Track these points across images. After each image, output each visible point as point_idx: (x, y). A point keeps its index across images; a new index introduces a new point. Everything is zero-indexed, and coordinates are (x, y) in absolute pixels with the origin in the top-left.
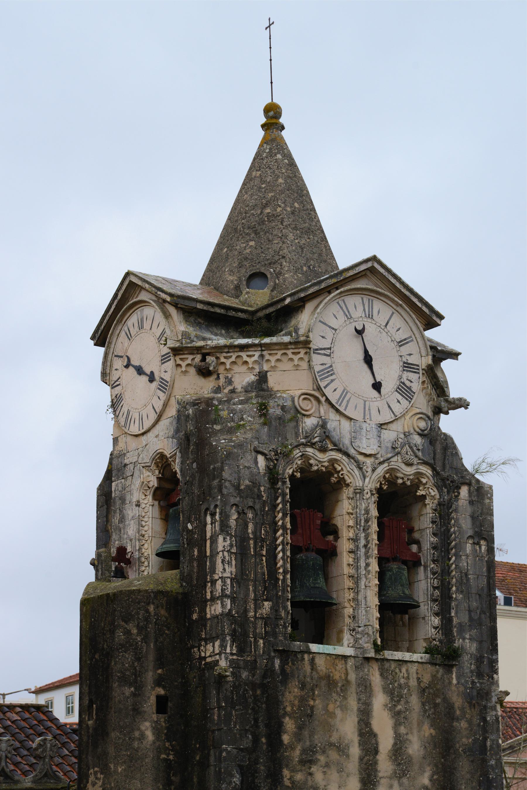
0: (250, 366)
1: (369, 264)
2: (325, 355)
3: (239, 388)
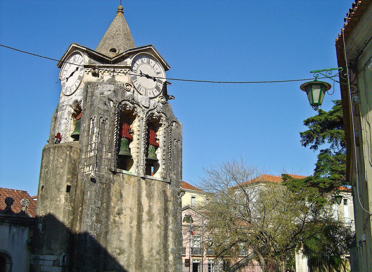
1: (150, 47)
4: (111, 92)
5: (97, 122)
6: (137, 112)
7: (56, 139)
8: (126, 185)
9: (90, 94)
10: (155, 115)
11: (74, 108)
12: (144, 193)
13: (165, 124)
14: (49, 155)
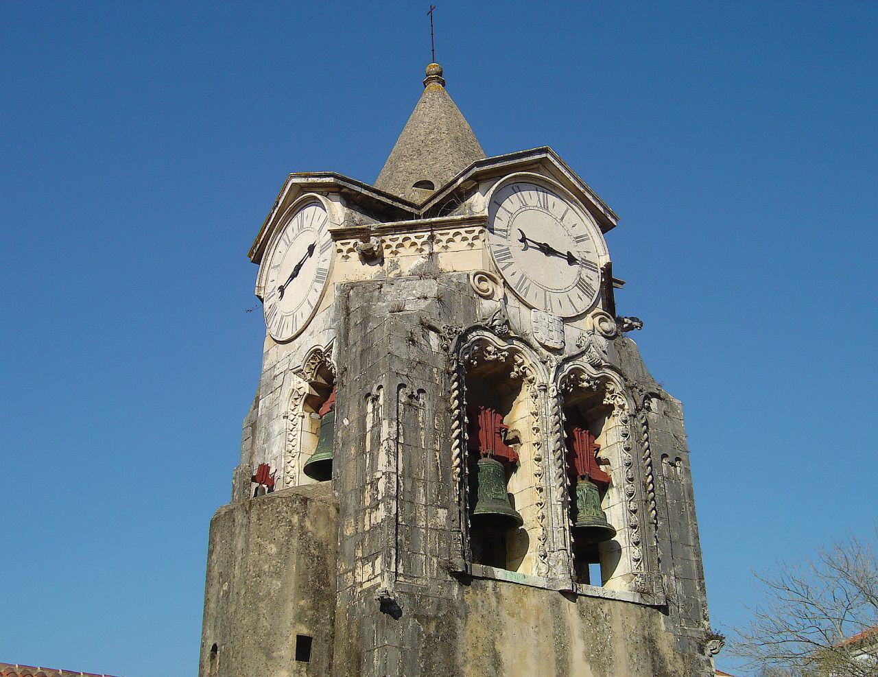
0: (419, 247)
1: (544, 155)
2: (501, 236)
3: (406, 273)
4: (429, 301)
5: (388, 401)
6: (524, 368)
7: (255, 485)
8: (511, 622)
9: (356, 319)
10: (585, 376)
11: (309, 377)
12: (578, 649)
13: (622, 407)
14: (232, 534)
